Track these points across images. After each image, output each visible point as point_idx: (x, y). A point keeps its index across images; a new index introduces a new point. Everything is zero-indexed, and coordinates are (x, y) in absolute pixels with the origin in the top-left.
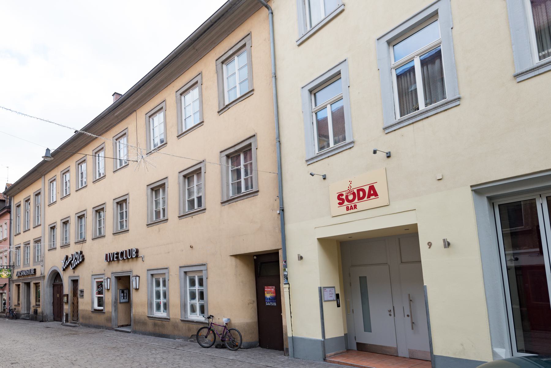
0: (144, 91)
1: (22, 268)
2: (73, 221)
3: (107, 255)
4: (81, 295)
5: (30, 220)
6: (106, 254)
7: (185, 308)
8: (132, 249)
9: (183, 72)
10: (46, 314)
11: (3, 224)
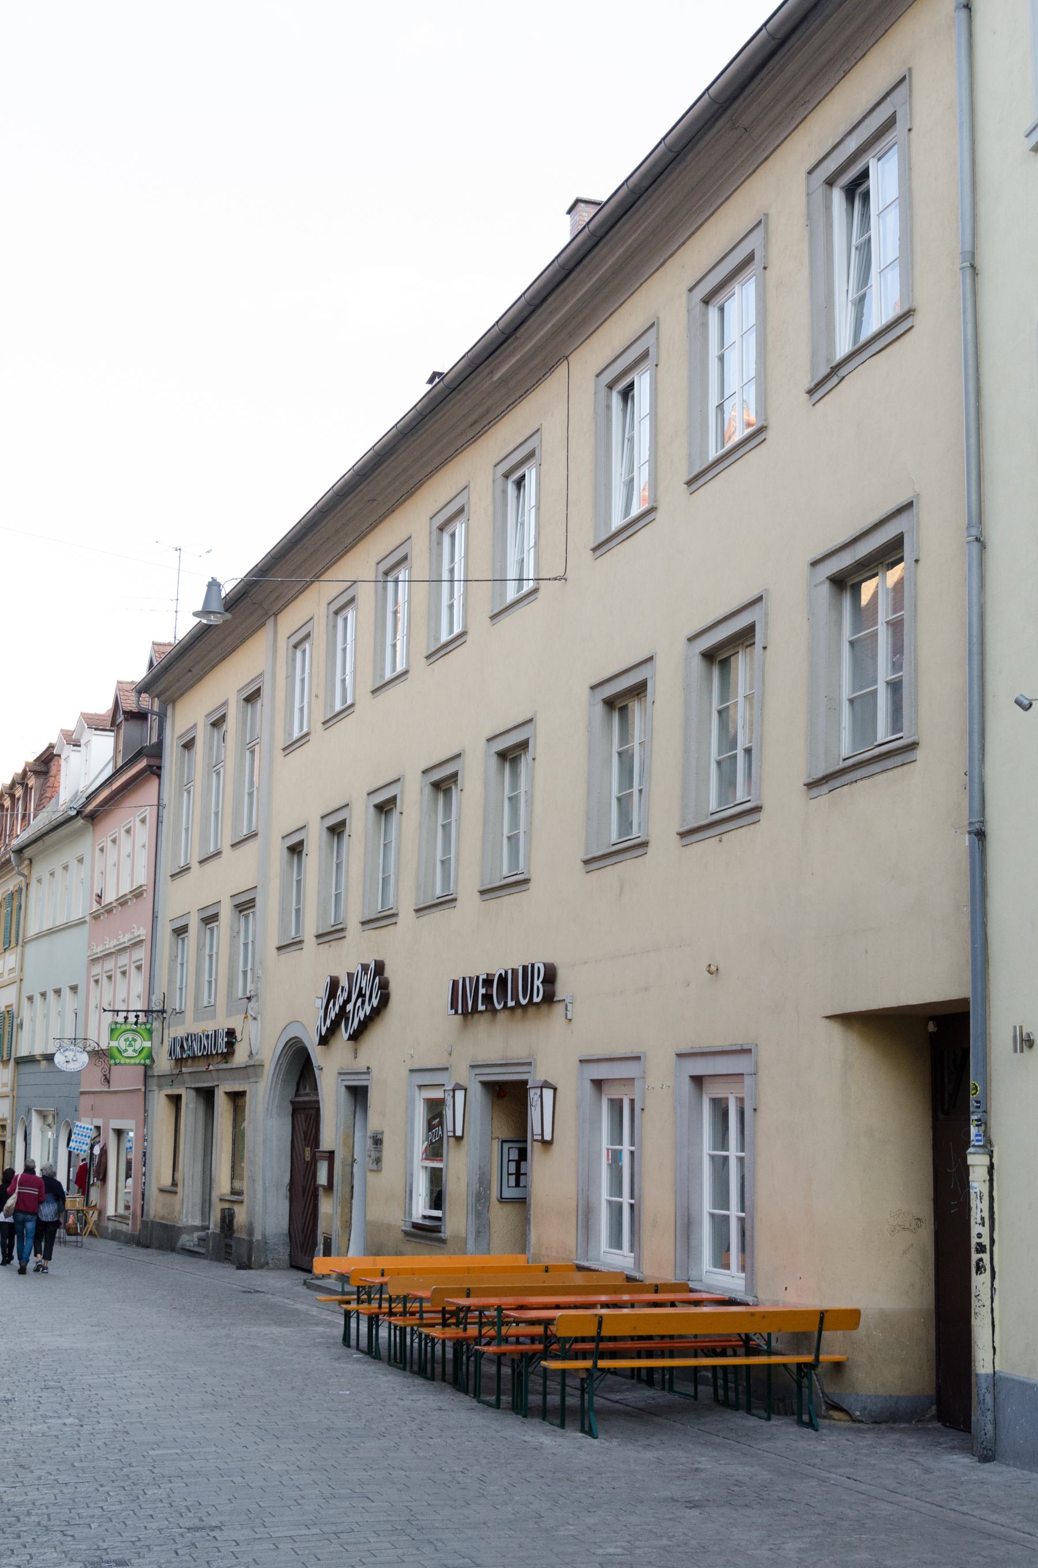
0: (585, 283)
1: (188, 1026)
2: (315, 840)
3: (455, 983)
6: (454, 981)
7: (688, 1238)
8: (533, 966)
9: (712, 210)
10: (264, 1235)
11: (120, 834)
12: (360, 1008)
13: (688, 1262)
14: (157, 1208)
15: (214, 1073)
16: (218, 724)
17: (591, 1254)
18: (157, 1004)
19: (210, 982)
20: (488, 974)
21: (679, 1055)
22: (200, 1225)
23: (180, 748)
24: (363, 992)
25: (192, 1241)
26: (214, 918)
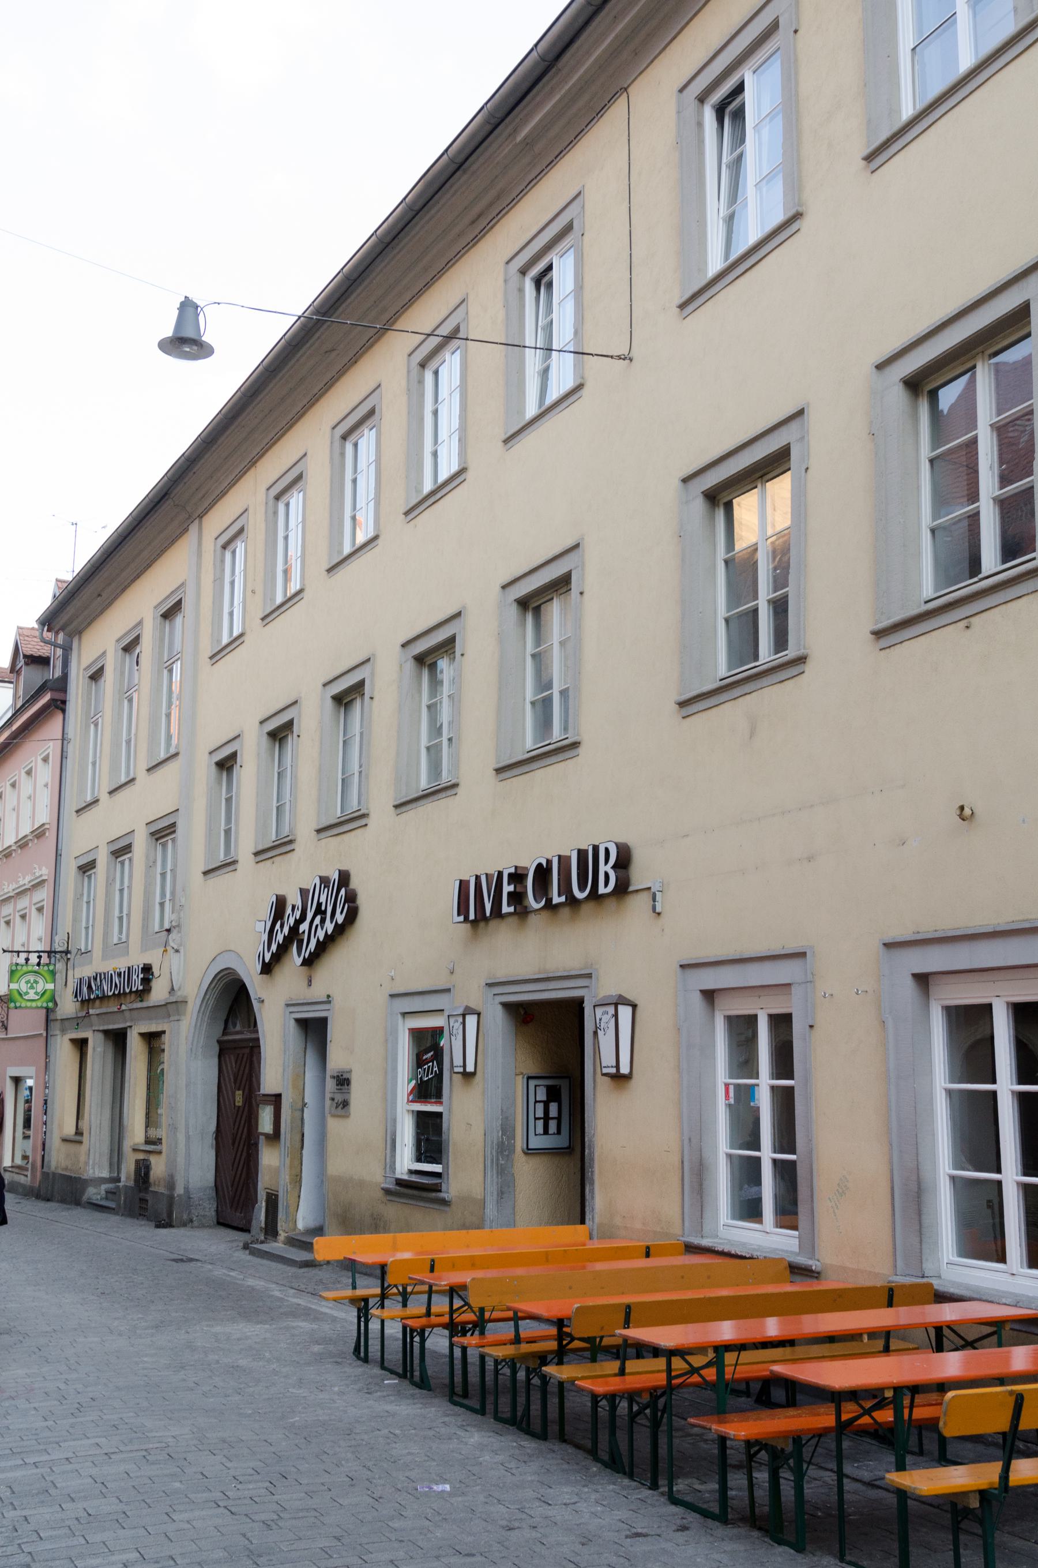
3: (463, 885)
4: (339, 1098)
5: (136, 735)
6: (461, 881)
8: (596, 849)
10: (186, 1189)
12: (319, 927)
13: (921, 1249)
14: (59, 1158)
15: (127, 1014)
16: (130, 648)
17: (707, 1228)
18: (61, 945)
19: (121, 918)
20: (516, 867)
21: (887, 945)
22: (108, 1177)
23: (87, 680)
24: (323, 908)
25: (99, 1194)
26: (127, 849)
